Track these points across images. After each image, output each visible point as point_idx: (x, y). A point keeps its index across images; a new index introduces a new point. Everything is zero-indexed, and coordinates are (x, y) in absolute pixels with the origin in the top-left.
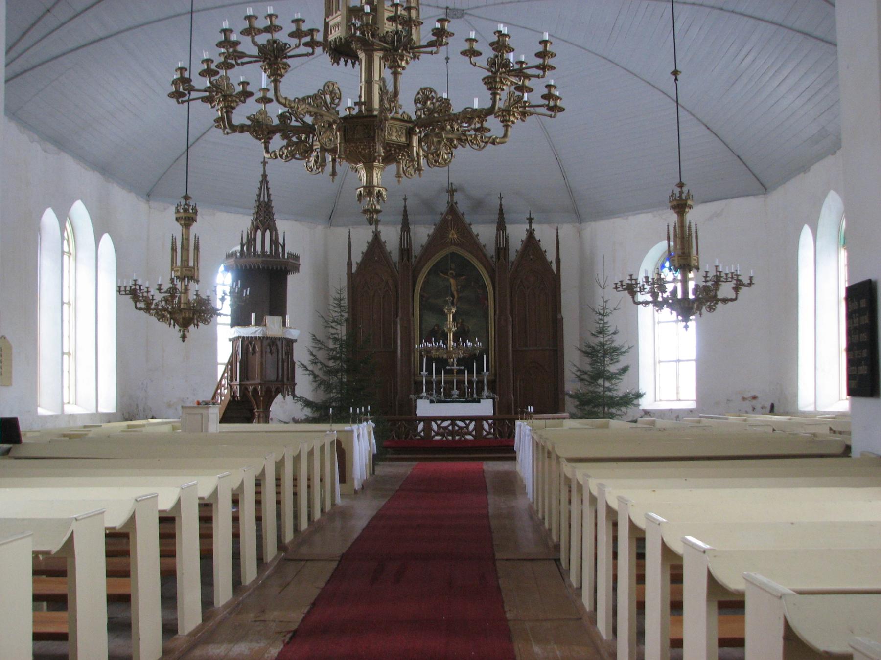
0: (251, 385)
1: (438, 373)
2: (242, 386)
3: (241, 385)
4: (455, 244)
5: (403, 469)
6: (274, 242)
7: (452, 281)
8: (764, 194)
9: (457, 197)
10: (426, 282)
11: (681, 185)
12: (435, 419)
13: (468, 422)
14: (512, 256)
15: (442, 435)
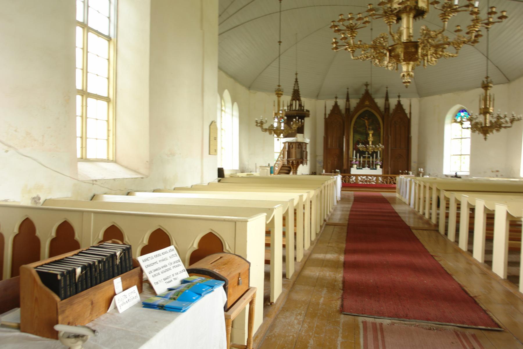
0: (291, 160)
1: (360, 158)
2: (288, 161)
3: (287, 160)
4: (368, 107)
5: (351, 194)
6: (300, 105)
7: (366, 121)
8: (508, 83)
9: (369, 87)
10: (356, 122)
11: (487, 77)
12: (360, 175)
13: (373, 177)
14: (391, 111)
15: (362, 182)
